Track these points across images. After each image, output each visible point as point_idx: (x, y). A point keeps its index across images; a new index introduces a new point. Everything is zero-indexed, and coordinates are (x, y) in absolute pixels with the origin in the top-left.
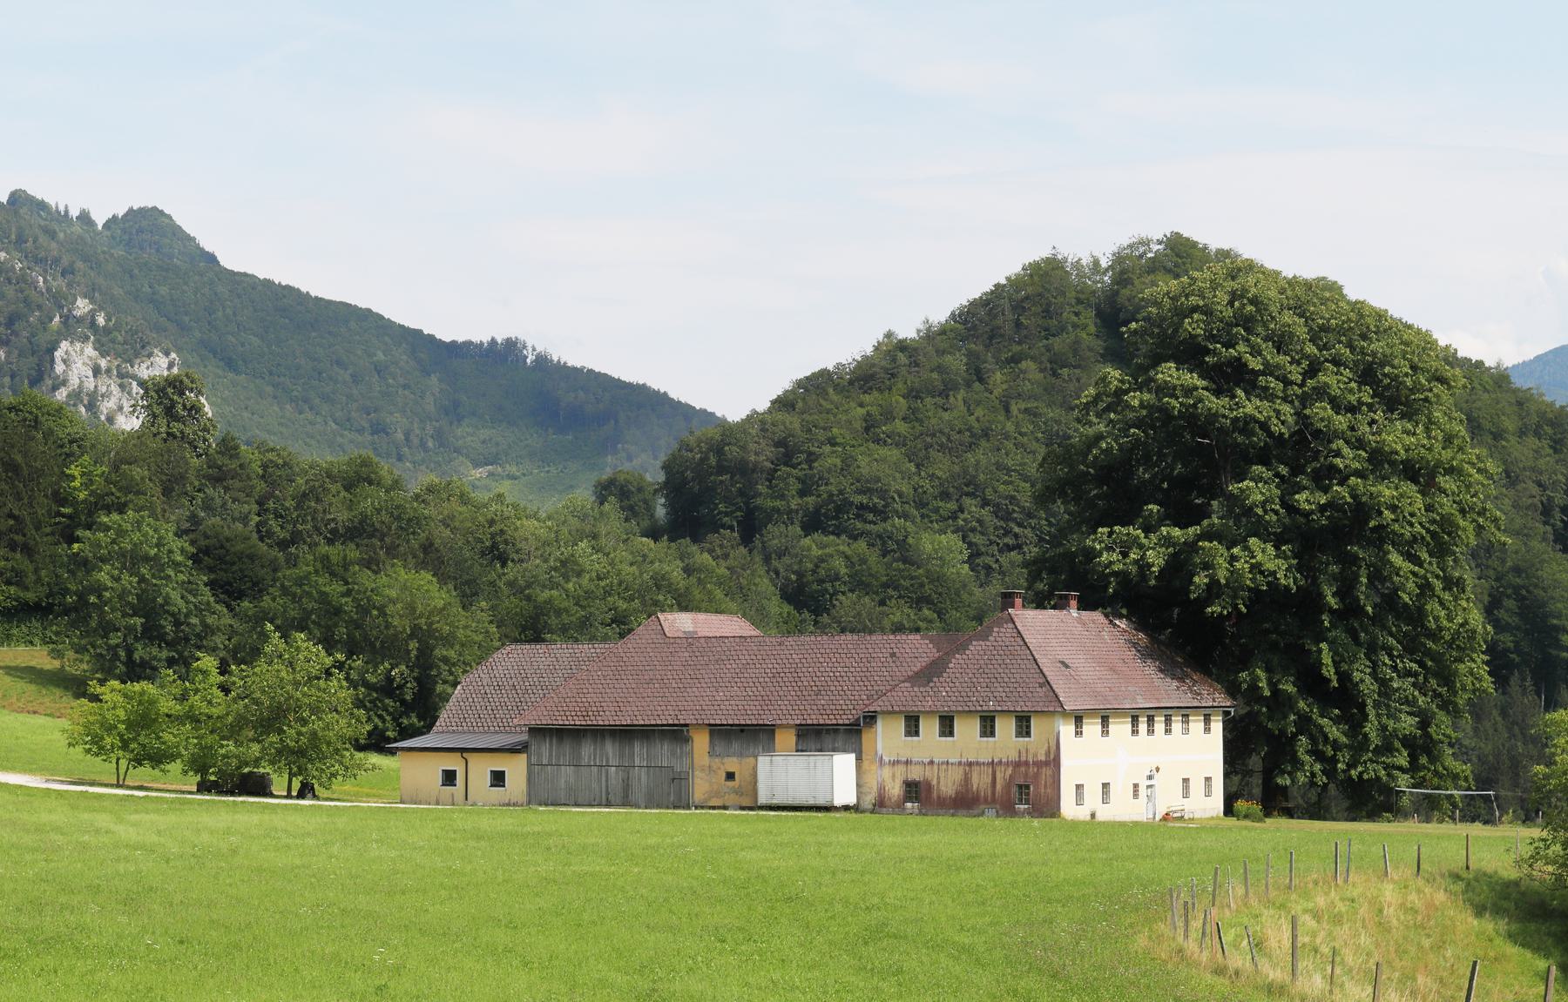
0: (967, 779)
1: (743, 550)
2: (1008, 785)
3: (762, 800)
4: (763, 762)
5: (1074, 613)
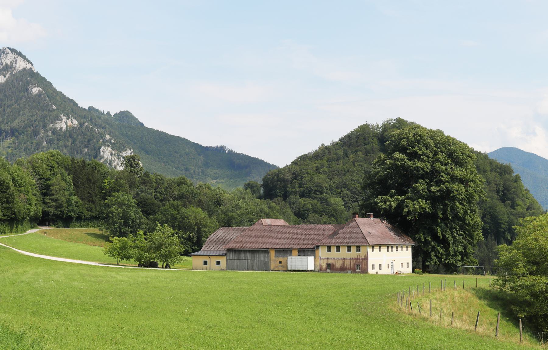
0: (343, 263)
3: (289, 269)
4: (289, 258)
5: (372, 219)
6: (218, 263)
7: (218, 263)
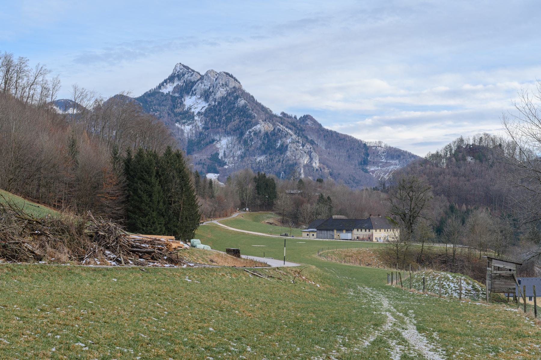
6: (313, 235)
7: (313, 235)
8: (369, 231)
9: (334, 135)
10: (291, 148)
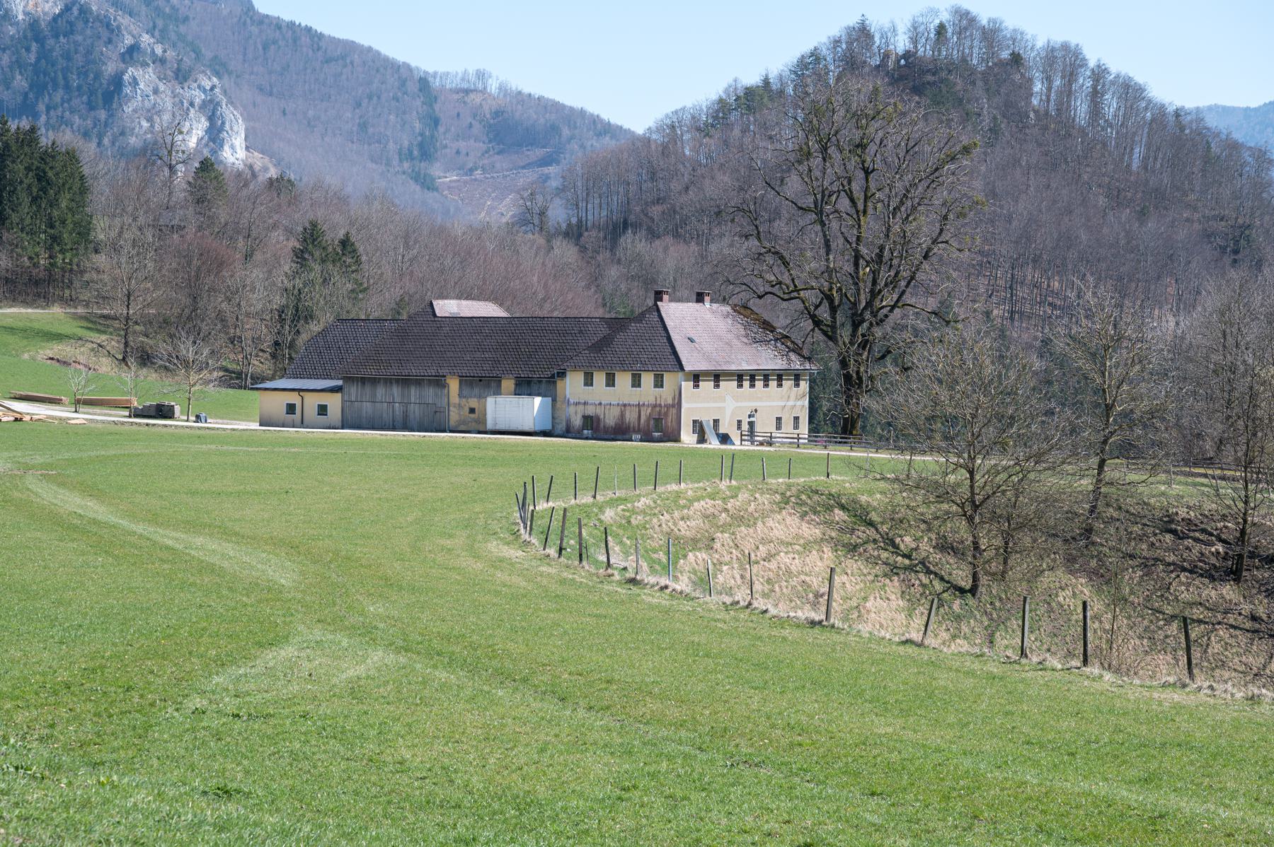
0: (622, 415)
1: (657, 242)
2: (648, 420)
3: (490, 426)
4: (490, 401)
5: (707, 305)
8: (659, 383)
9: (305, 40)
10: (135, 82)
